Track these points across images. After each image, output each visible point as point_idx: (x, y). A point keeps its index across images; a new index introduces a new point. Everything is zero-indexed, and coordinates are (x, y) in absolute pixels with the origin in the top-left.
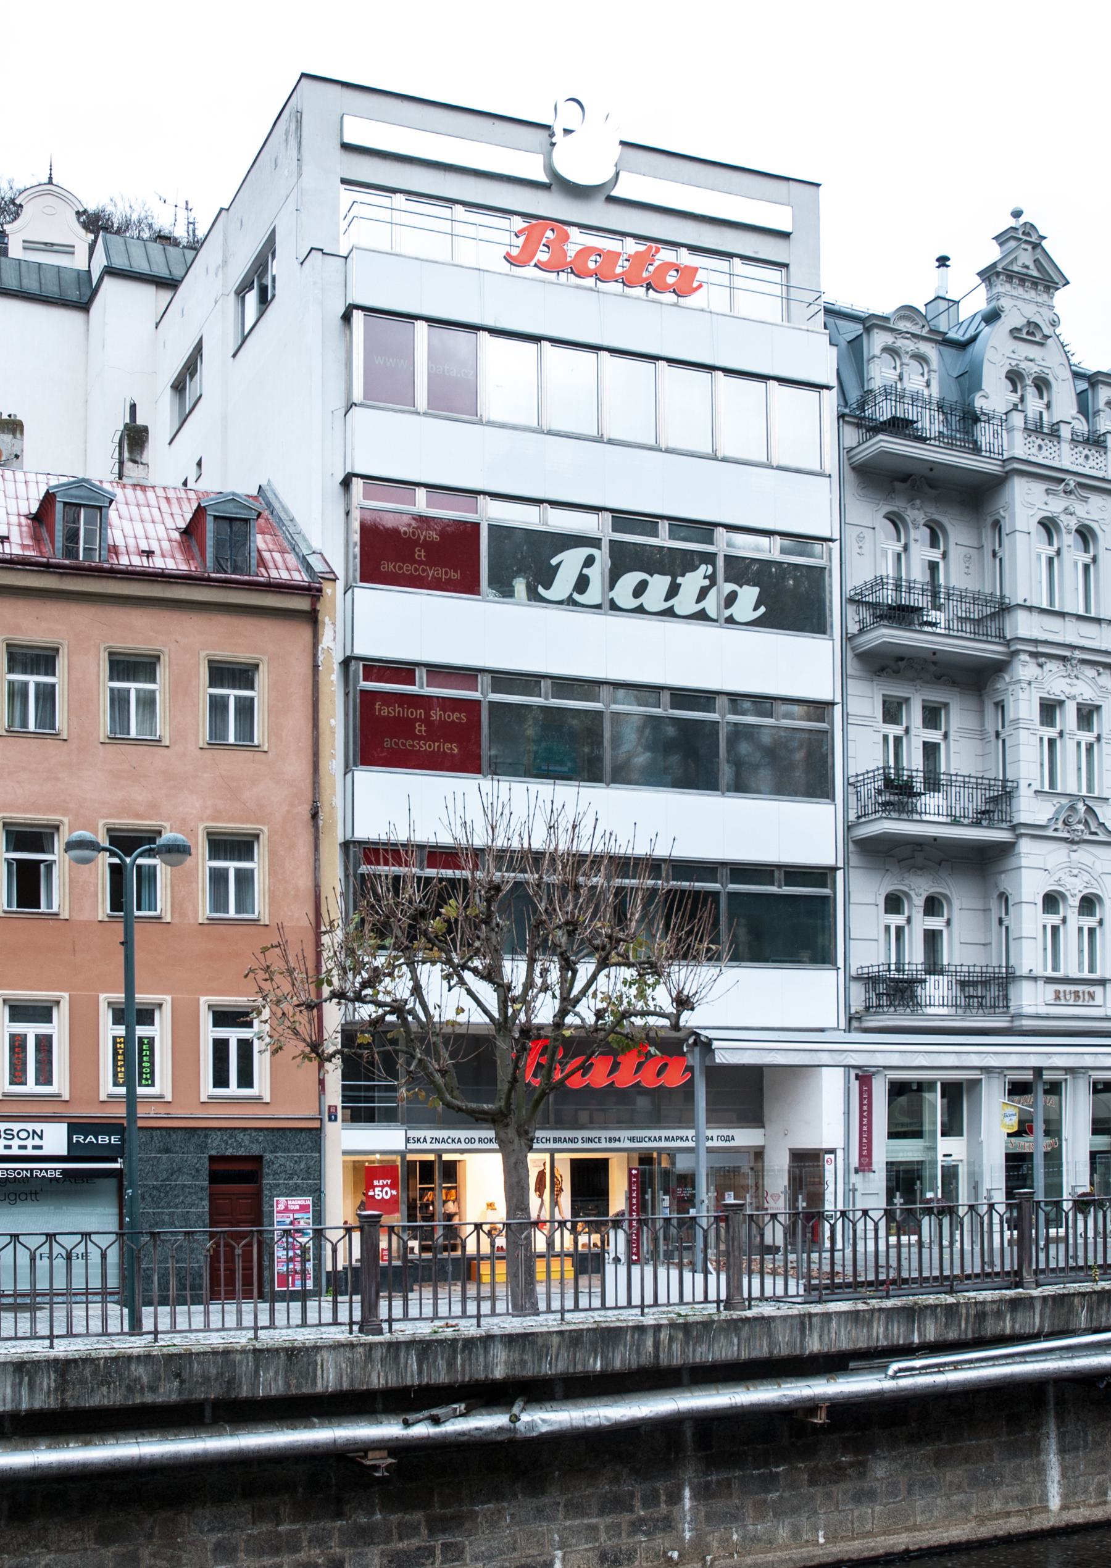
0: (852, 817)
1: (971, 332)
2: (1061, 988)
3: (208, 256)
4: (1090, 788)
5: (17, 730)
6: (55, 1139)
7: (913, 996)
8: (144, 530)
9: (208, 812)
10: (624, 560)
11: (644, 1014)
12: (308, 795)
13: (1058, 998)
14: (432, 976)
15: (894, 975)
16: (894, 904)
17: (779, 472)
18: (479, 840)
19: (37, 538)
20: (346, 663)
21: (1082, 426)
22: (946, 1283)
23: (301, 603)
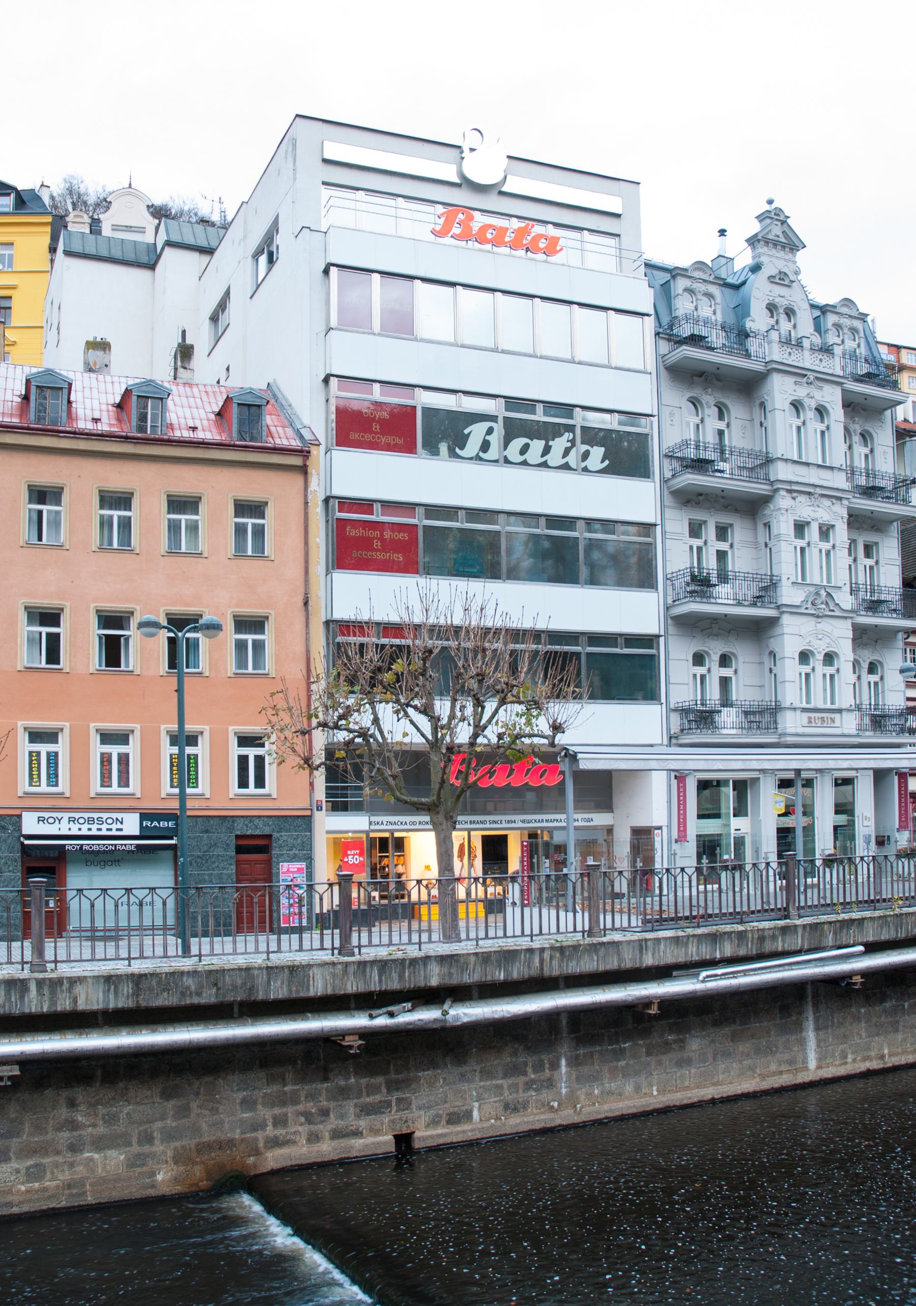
0: (670, 601)
2: (812, 715)
4: (829, 581)
5: (105, 547)
6: (131, 824)
8: (190, 412)
10: (513, 430)
11: (530, 736)
12: (301, 590)
13: (810, 722)
14: (386, 711)
15: (699, 707)
16: (699, 659)
19: (119, 420)
20: (327, 500)
21: (817, 340)
22: (738, 916)
23: (297, 461)
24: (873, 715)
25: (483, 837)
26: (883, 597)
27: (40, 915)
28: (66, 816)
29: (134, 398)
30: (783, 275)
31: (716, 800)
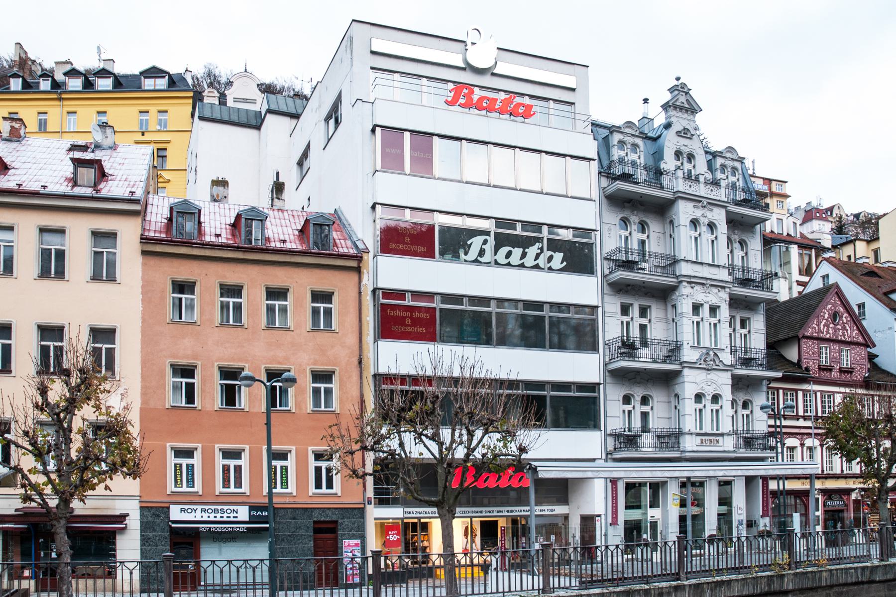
0: (607, 360)
1: (659, 133)
3: (311, 104)
4: (716, 344)
5: (224, 324)
6: (243, 513)
7: (636, 443)
8: (281, 230)
9: (312, 361)
10: (501, 241)
11: (506, 455)
12: (357, 353)
14: (408, 438)
15: (627, 433)
16: (627, 400)
17: (572, 200)
18: (429, 372)
19: (233, 235)
20: (374, 291)
21: (709, 176)
22: (645, 579)
23: (353, 264)
24: (745, 438)
25: (481, 522)
26: (753, 356)
27: (169, 575)
28: (200, 507)
29: (243, 220)
30: (686, 130)
31: (638, 497)
